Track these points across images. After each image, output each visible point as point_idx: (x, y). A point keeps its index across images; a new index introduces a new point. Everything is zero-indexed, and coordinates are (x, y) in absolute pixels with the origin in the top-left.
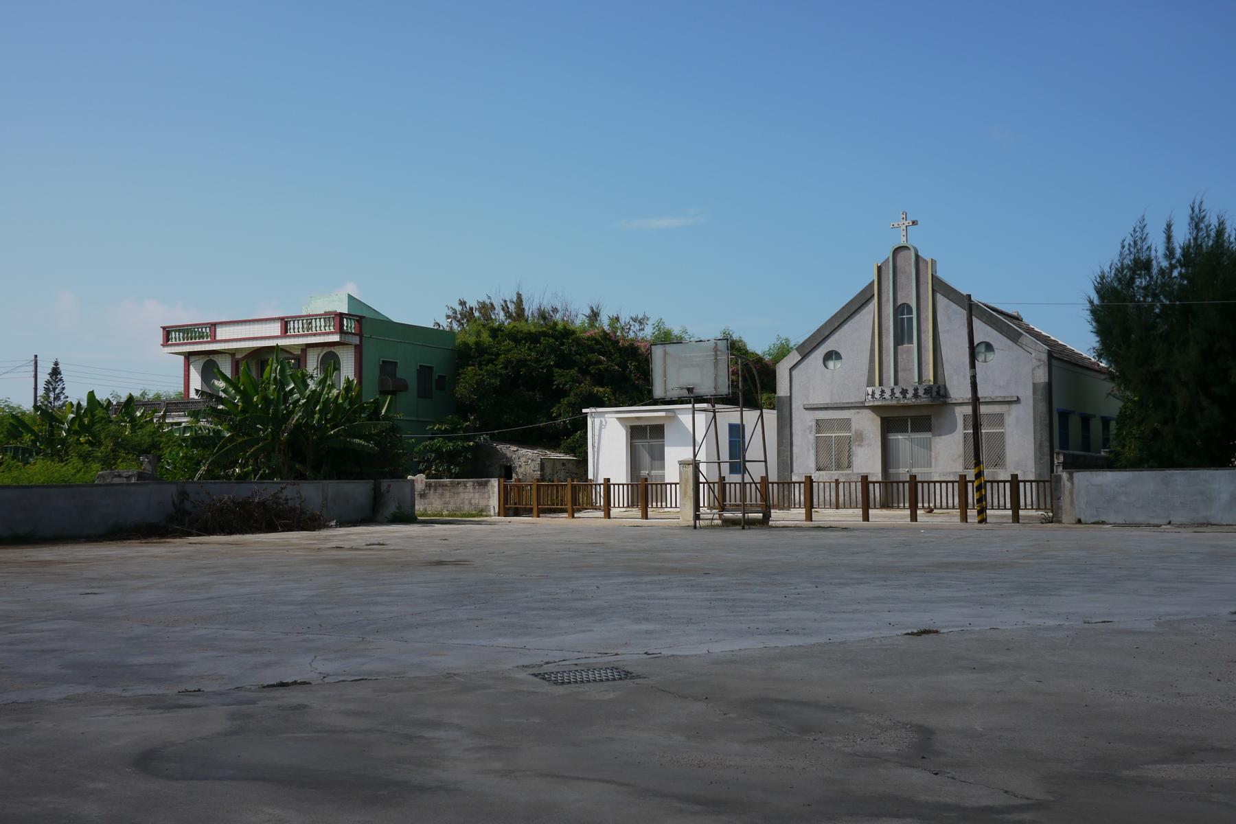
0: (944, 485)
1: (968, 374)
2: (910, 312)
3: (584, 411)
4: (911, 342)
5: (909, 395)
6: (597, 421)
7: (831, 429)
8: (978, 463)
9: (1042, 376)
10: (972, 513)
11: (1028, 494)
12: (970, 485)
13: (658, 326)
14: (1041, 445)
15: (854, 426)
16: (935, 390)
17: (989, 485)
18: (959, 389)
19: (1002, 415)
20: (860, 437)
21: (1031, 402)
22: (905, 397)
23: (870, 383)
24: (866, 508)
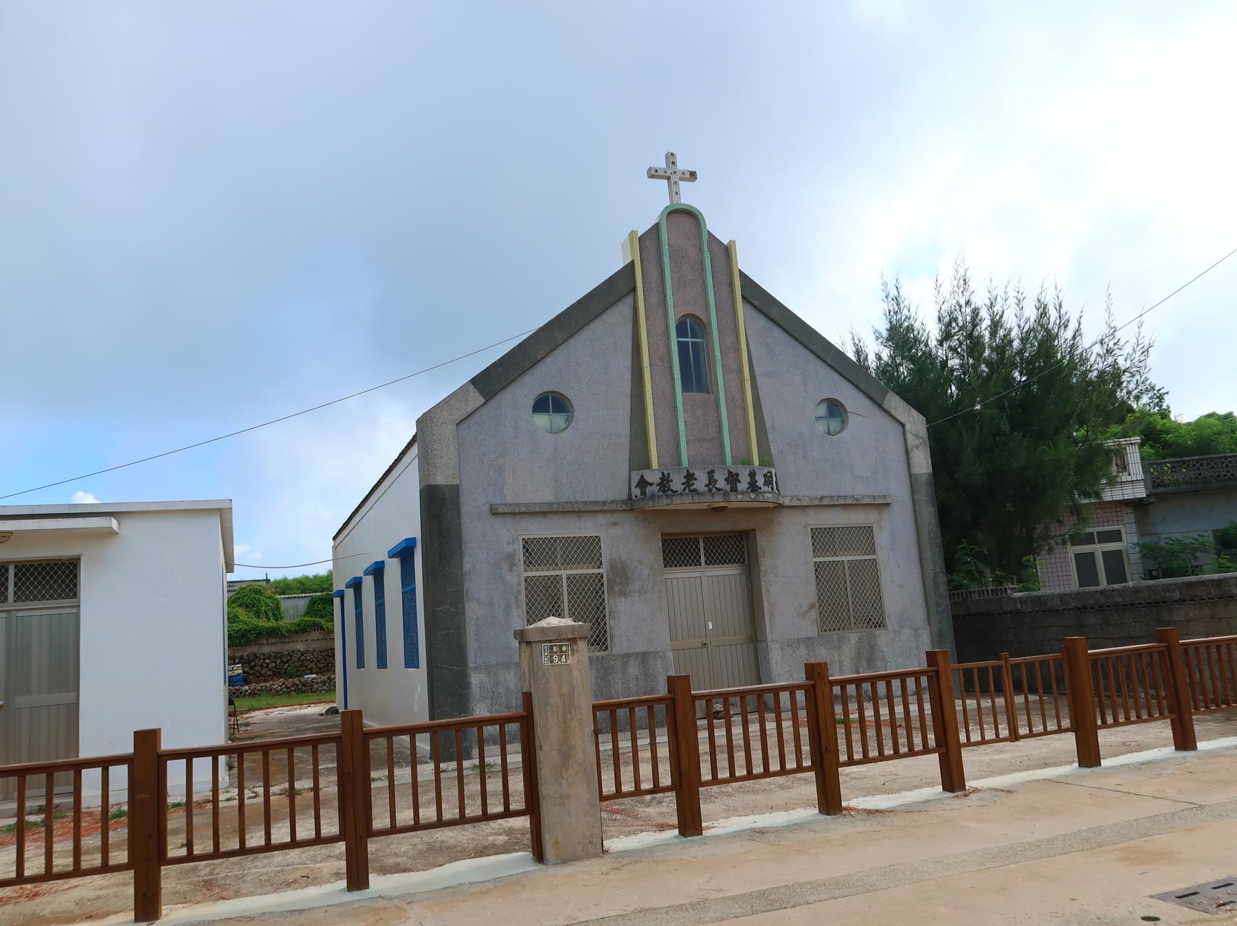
20: (622, 576)
22: (734, 489)
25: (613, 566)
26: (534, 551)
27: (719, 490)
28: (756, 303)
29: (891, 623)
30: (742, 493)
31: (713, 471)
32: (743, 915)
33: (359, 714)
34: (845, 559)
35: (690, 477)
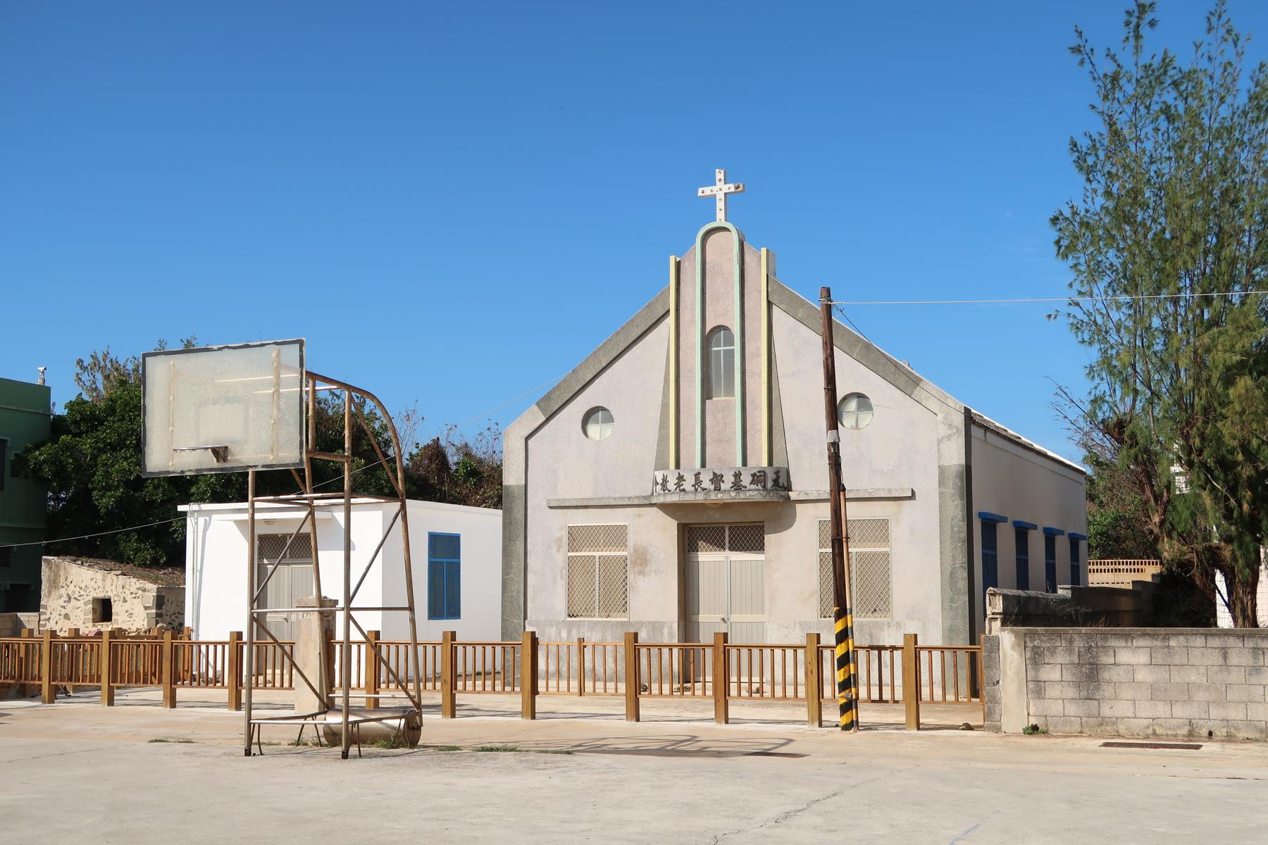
0: (778, 652)
1: (826, 437)
2: (730, 341)
3: (181, 508)
4: (730, 392)
5: (727, 484)
6: (201, 520)
7: (594, 545)
8: (842, 613)
9: (955, 455)
10: (832, 715)
11: (931, 667)
12: (827, 654)
14: (952, 575)
15: (632, 540)
16: (771, 476)
17: (862, 654)
18: (809, 478)
19: (885, 523)
22: (718, 489)
23: (661, 464)
24: (637, 688)
25: (636, 550)
26: (576, 537)
32: (1257, 740)
34: (597, 554)
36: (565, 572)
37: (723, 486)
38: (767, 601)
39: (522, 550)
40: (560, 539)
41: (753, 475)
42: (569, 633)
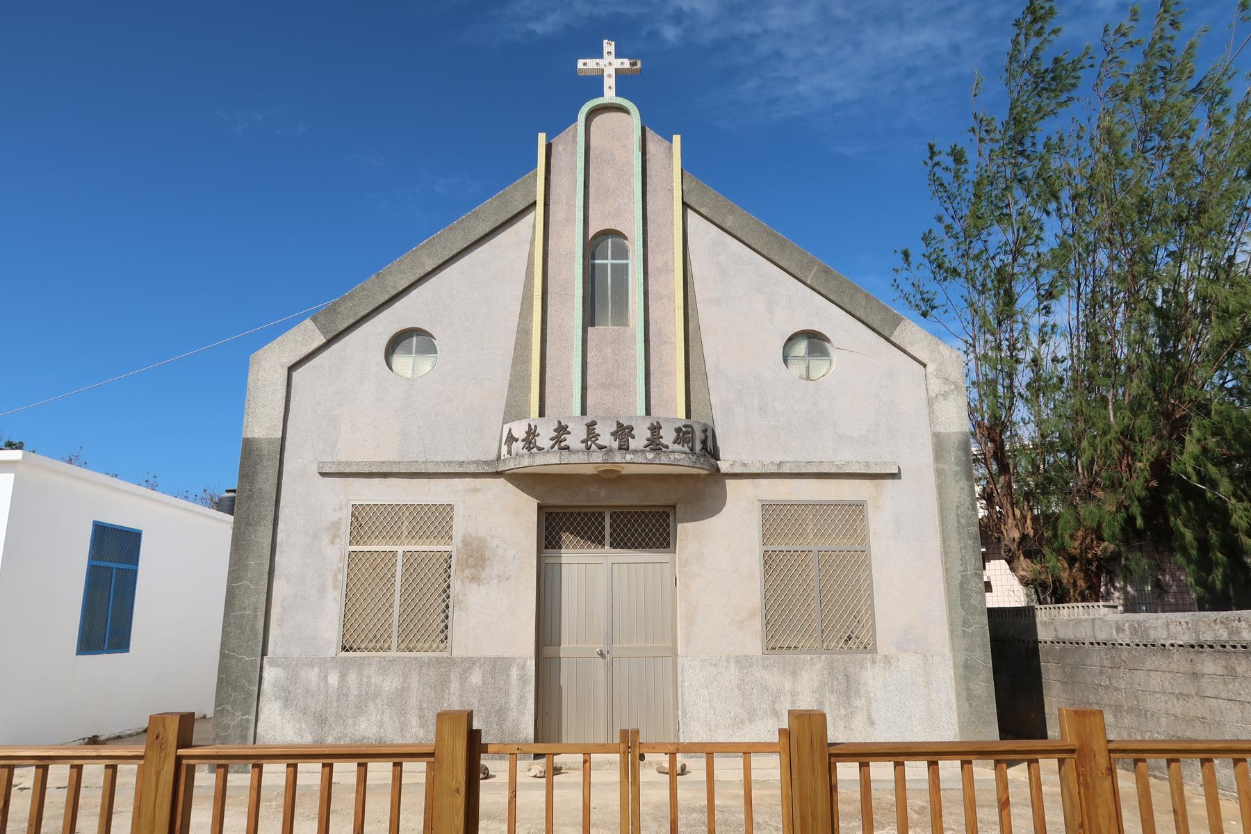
2: (622, 253)
4: (621, 316)
13: (983, 126)
15: (460, 528)
20: (477, 557)
21: (930, 479)
22: (624, 448)
23: (514, 411)
25: (466, 543)
26: (363, 521)
27: (601, 448)
28: (702, 211)
29: (885, 644)
30: (635, 452)
31: (594, 423)
33: (479, 732)
34: (400, 549)
35: (562, 430)
36: (342, 577)
37: (633, 444)
38: (680, 623)
39: (268, 541)
40: (336, 525)
41: (678, 430)
42: (343, 676)
